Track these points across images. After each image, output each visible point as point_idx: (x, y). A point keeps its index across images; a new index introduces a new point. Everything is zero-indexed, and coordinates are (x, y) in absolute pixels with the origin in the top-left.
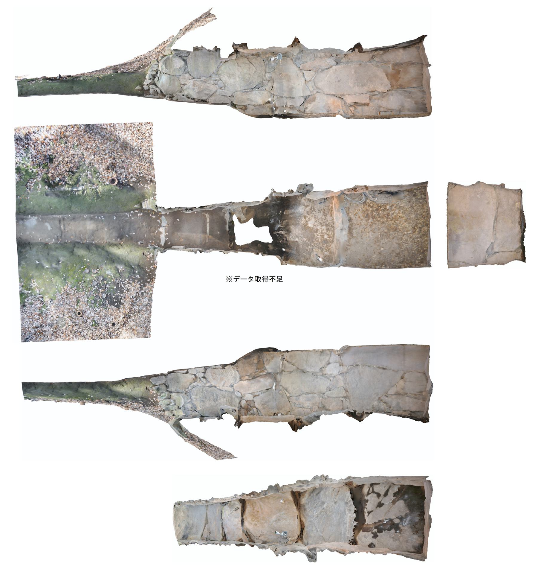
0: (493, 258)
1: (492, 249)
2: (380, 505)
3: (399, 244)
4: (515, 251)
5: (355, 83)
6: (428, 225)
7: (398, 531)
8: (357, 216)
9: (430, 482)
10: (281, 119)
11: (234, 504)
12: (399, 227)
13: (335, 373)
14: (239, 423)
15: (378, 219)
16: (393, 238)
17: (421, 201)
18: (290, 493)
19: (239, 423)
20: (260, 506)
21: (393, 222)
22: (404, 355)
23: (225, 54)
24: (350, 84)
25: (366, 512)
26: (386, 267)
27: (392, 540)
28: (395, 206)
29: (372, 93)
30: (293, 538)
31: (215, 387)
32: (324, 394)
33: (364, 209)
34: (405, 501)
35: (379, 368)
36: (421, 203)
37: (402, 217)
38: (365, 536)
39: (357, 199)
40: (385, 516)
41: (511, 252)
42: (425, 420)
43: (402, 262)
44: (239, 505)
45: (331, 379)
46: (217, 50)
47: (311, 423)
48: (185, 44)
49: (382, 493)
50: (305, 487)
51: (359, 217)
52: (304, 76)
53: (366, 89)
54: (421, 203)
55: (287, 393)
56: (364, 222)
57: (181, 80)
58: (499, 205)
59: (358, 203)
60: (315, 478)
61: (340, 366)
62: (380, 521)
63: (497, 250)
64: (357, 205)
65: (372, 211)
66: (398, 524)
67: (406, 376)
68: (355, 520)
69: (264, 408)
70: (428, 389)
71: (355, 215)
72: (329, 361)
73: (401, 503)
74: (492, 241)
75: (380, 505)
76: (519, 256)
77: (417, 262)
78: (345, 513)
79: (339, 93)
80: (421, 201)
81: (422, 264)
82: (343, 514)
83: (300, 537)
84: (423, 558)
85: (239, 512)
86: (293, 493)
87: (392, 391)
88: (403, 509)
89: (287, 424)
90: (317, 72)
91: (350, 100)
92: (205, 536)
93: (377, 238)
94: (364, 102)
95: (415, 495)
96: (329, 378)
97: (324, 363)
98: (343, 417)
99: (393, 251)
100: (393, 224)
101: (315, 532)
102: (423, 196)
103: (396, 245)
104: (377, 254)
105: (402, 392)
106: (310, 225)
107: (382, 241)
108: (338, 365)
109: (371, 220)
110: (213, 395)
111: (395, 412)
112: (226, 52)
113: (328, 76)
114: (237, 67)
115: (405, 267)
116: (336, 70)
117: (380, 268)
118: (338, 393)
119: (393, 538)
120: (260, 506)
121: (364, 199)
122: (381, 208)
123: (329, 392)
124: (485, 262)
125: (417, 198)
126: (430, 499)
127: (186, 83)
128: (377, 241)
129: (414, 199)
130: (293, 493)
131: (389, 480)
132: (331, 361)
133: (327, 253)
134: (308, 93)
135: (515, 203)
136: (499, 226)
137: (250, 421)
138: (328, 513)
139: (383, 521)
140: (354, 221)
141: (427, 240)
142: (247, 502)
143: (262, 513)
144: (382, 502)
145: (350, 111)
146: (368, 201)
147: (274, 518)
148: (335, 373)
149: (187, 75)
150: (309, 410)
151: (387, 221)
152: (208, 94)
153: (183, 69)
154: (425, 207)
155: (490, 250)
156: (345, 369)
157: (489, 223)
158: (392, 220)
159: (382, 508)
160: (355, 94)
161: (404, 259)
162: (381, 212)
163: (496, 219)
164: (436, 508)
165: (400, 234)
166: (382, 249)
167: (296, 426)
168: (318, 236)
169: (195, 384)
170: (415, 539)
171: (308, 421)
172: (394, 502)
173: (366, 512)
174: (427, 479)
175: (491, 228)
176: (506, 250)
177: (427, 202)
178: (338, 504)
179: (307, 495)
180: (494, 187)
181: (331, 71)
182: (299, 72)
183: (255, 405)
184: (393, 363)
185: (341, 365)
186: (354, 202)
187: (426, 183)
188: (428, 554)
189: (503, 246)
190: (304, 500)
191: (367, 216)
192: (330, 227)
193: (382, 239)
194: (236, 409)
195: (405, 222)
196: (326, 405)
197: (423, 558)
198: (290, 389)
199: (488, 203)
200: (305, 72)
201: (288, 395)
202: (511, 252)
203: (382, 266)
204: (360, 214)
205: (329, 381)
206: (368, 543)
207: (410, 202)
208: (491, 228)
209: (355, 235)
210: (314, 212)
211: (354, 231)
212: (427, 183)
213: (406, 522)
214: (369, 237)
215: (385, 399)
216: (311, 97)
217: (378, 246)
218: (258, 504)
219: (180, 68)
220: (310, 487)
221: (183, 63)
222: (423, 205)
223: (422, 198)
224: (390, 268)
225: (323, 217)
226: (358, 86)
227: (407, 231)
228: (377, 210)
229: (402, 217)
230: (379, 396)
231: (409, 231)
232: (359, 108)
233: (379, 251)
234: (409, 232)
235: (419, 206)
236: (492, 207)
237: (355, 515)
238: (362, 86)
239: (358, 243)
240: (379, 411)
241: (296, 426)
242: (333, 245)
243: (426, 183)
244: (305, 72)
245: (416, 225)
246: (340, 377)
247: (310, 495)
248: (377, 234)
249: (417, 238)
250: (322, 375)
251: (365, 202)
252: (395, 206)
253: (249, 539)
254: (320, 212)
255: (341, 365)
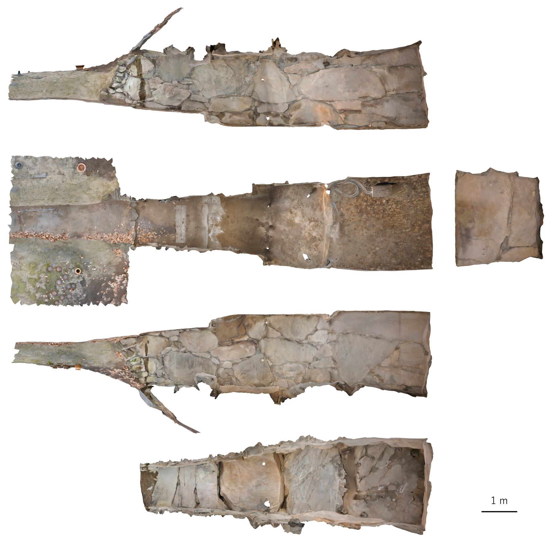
0: (507, 255)
1: (507, 244)
2: (373, 470)
3: (396, 243)
4: (532, 246)
5: (345, 88)
6: (429, 222)
7: (394, 500)
8: (350, 212)
9: (430, 444)
10: (238, 519)
11: (209, 466)
12: (396, 225)
13: (323, 341)
14: (215, 394)
15: (374, 215)
16: (390, 237)
17: (421, 194)
18: (273, 455)
19: (215, 394)
20: (239, 469)
21: (389, 218)
22: (400, 323)
23: (200, 54)
24: (339, 90)
25: (358, 477)
26: (381, 269)
27: (387, 509)
28: (392, 200)
29: (363, 100)
30: (276, 506)
31: (191, 352)
32: (310, 364)
33: (358, 204)
34: (402, 465)
35: (371, 337)
36: (421, 197)
37: (400, 213)
38: (356, 505)
39: (350, 193)
40: (379, 482)
41: (528, 247)
42: (425, 395)
43: (400, 263)
44: (215, 468)
45: (319, 347)
46: (191, 50)
47: (295, 396)
48: (156, 45)
49: (377, 456)
50: (290, 449)
51: (352, 213)
52: (288, 80)
53: (358, 94)
54: (421, 197)
55: (269, 361)
56: (357, 218)
57: (151, 84)
58: (514, 195)
59: (351, 196)
60: (301, 438)
61: (328, 333)
62: (374, 487)
63: (512, 245)
64: (349, 199)
65: (366, 206)
66: (393, 492)
67: (402, 347)
68: (345, 487)
69: (244, 378)
70: (428, 361)
71: (347, 210)
72: (316, 327)
73: (397, 468)
74: (507, 235)
75: (373, 470)
76: (537, 253)
77: (417, 263)
78: (335, 478)
79: (327, 98)
80: (421, 194)
81: (422, 266)
82: (331, 481)
83: (283, 506)
84: (421, 530)
85: (216, 474)
86: (276, 455)
87: (386, 363)
88: (399, 478)
89: (268, 395)
90: (302, 76)
91: (339, 106)
92: (177, 501)
93: (371, 236)
94: (355, 109)
95: (414, 458)
96: (315, 347)
97: (311, 330)
98: (329, 389)
99: (389, 251)
100: (389, 220)
101: (300, 499)
102: (424, 189)
103: (393, 244)
104: (371, 253)
105: (396, 364)
106: (297, 220)
107: (378, 240)
108: (326, 332)
109: (365, 216)
110: (188, 362)
111: (389, 386)
112: (200, 54)
113: (314, 81)
114: (213, 70)
115: (403, 269)
116: (323, 75)
117: (375, 270)
118: (325, 364)
119: (388, 507)
120: (239, 469)
121: (357, 192)
122: (376, 202)
123: (316, 362)
124: (498, 259)
125: (417, 192)
126: (430, 465)
127: (155, 87)
128: (371, 239)
129: (413, 193)
130: (276, 455)
131: (384, 442)
132: (318, 328)
133: (315, 253)
134: (293, 99)
135: (532, 192)
136: (515, 218)
137: (229, 391)
138: (315, 478)
139: (377, 487)
140: (346, 217)
141: (428, 239)
142: (224, 467)
143: (241, 477)
144: (377, 466)
145: (339, 119)
146: (362, 194)
147: (254, 482)
148: (323, 341)
149: (157, 78)
150: (292, 382)
151: (383, 217)
152: (180, 100)
153: (152, 73)
154: (425, 201)
155: (504, 245)
156: (334, 337)
157: (502, 215)
158: (388, 216)
159: (376, 473)
160: (346, 101)
161: (402, 260)
162: (376, 207)
163: (510, 211)
164: (435, 475)
165: (398, 232)
166: (378, 249)
167: (278, 399)
168: (305, 234)
169: (168, 348)
170: (413, 508)
171: (292, 393)
172: (389, 467)
173: (358, 477)
174: (428, 441)
175: (501, 218)
176: (522, 245)
177: (428, 196)
178: (326, 468)
179: (291, 457)
180: (509, 175)
181: (318, 76)
182: (282, 75)
183: (234, 373)
184: (389, 333)
185: (331, 332)
186: (346, 195)
187: (428, 174)
188: (427, 527)
189: (519, 240)
190: (287, 464)
191: (361, 212)
192: (318, 223)
193: (377, 237)
194: (214, 377)
195: (404, 218)
196: (312, 376)
197: (421, 530)
198: (273, 358)
199: (502, 193)
200: (289, 75)
201: (271, 364)
202: (528, 247)
203: (377, 267)
204: (353, 209)
205: (316, 350)
206: (360, 513)
207: (408, 196)
208: (501, 218)
209: (346, 233)
210: (301, 206)
211: (346, 228)
212: (429, 174)
213: (403, 490)
214: (362, 235)
215: (377, 372)
216: (296, 104)
217: (373, 245)
218: (236, 467)
219: (149, 71)
220: (295, 448)
221: (153, 66)
222: (424, 200)
223: (422, 192)
224: (386, 270)
225: (312, 212)
226: (348, 91)
227: (405, 229)
228: (372, 204)
229: (400, 213)
230: (372, 368)
231: (408, 229)
232: (350, 116)
233: (374, 251)
234: (407, 230)
235: (419, 200)
236: (507, 197)
237: (345, 481)
238: (354, 91)
239: (350, 241)
240: (371, 384)
241: (278, 399)
242: (322, 244)
243: (428, 174)
244: (289, 75)
245: (416, 223)
246: (328, 345)
247: (295, 457)
248: (372, 231)
249: (417, 236)
250: (309, 343)
251: (358, 197)
252: (392, 200)
253: (226, 505)
254: (307, 206)
255: (331, 332)
